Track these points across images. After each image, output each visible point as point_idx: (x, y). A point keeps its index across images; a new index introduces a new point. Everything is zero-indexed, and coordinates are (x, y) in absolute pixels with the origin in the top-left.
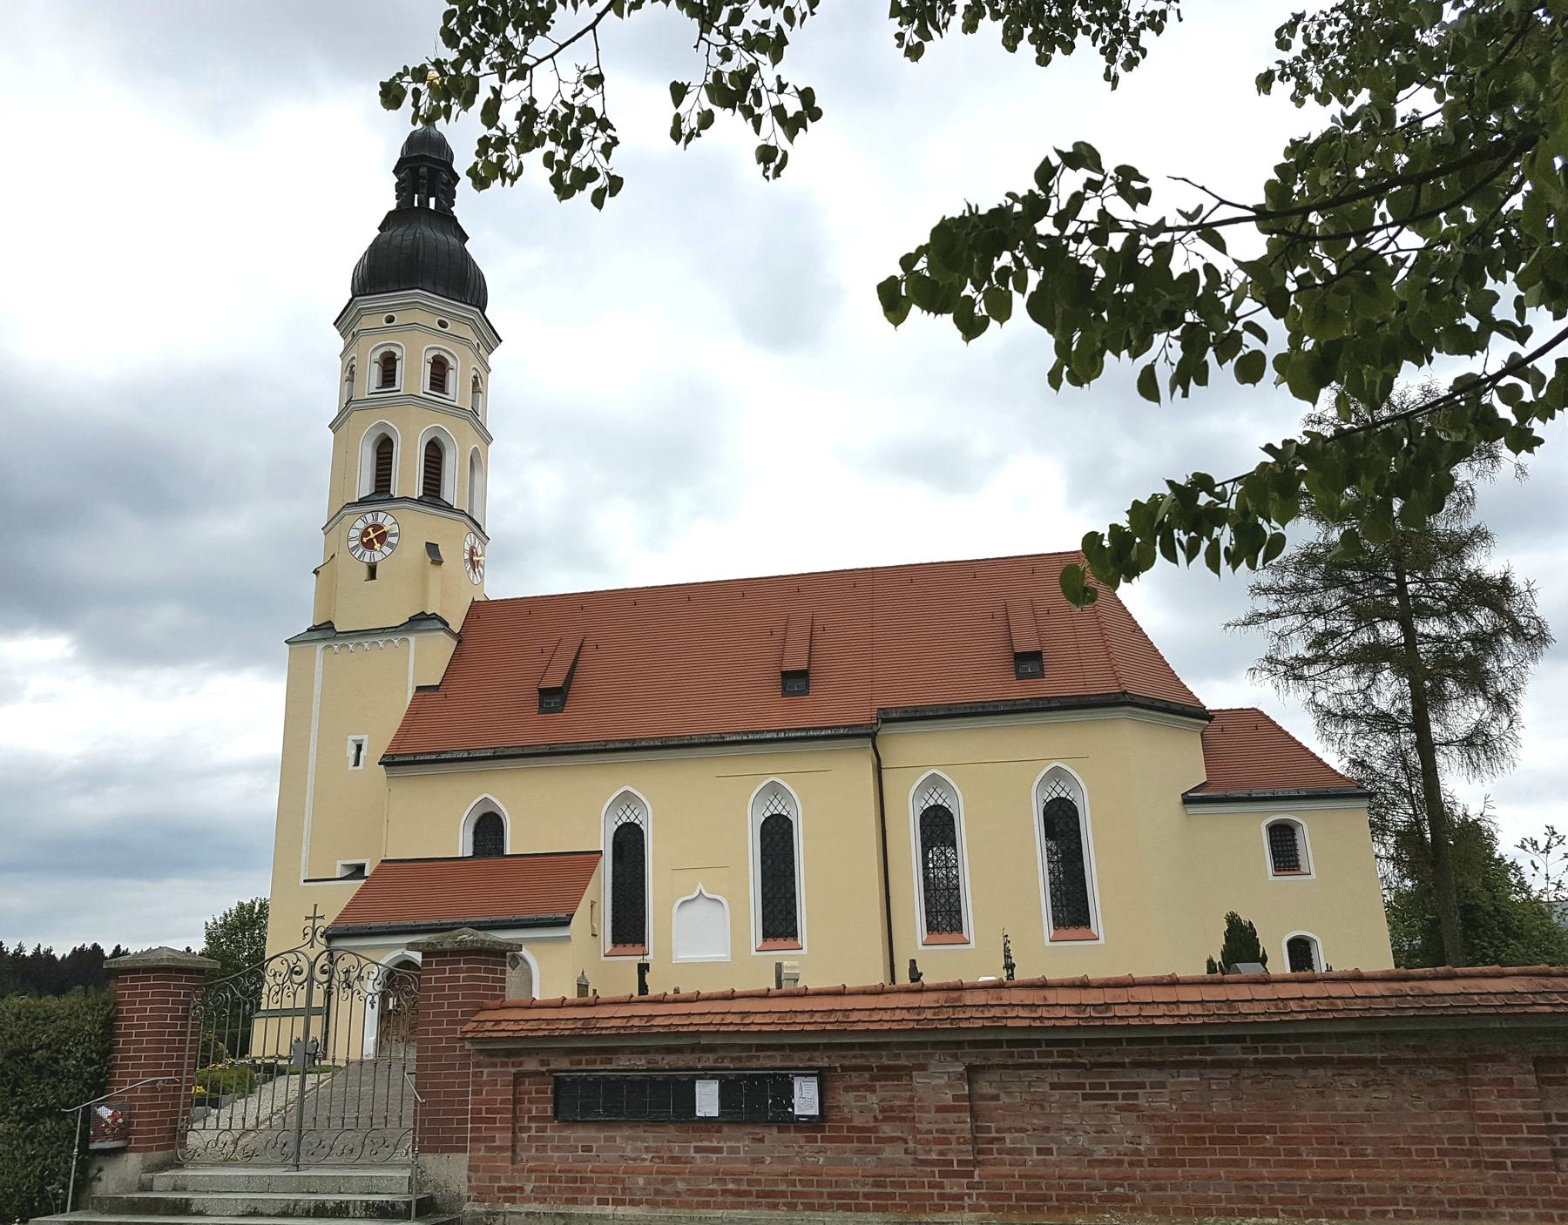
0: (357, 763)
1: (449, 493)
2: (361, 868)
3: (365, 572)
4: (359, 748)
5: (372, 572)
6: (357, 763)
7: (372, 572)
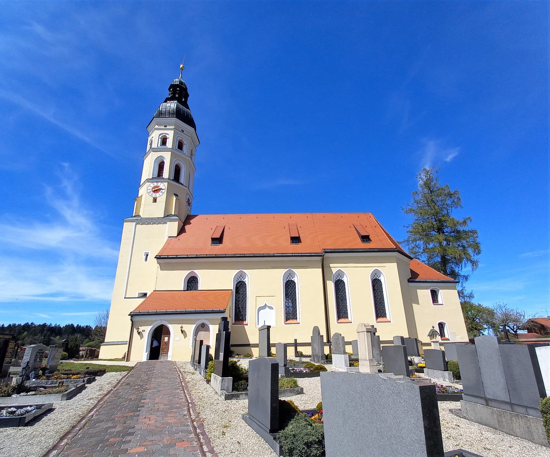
0: (146, 259)
1: (182, 179)
2: (145, 295)
4: (147, 255)
5: (155, 200)
6: (146, 259)
7: (155, 200)
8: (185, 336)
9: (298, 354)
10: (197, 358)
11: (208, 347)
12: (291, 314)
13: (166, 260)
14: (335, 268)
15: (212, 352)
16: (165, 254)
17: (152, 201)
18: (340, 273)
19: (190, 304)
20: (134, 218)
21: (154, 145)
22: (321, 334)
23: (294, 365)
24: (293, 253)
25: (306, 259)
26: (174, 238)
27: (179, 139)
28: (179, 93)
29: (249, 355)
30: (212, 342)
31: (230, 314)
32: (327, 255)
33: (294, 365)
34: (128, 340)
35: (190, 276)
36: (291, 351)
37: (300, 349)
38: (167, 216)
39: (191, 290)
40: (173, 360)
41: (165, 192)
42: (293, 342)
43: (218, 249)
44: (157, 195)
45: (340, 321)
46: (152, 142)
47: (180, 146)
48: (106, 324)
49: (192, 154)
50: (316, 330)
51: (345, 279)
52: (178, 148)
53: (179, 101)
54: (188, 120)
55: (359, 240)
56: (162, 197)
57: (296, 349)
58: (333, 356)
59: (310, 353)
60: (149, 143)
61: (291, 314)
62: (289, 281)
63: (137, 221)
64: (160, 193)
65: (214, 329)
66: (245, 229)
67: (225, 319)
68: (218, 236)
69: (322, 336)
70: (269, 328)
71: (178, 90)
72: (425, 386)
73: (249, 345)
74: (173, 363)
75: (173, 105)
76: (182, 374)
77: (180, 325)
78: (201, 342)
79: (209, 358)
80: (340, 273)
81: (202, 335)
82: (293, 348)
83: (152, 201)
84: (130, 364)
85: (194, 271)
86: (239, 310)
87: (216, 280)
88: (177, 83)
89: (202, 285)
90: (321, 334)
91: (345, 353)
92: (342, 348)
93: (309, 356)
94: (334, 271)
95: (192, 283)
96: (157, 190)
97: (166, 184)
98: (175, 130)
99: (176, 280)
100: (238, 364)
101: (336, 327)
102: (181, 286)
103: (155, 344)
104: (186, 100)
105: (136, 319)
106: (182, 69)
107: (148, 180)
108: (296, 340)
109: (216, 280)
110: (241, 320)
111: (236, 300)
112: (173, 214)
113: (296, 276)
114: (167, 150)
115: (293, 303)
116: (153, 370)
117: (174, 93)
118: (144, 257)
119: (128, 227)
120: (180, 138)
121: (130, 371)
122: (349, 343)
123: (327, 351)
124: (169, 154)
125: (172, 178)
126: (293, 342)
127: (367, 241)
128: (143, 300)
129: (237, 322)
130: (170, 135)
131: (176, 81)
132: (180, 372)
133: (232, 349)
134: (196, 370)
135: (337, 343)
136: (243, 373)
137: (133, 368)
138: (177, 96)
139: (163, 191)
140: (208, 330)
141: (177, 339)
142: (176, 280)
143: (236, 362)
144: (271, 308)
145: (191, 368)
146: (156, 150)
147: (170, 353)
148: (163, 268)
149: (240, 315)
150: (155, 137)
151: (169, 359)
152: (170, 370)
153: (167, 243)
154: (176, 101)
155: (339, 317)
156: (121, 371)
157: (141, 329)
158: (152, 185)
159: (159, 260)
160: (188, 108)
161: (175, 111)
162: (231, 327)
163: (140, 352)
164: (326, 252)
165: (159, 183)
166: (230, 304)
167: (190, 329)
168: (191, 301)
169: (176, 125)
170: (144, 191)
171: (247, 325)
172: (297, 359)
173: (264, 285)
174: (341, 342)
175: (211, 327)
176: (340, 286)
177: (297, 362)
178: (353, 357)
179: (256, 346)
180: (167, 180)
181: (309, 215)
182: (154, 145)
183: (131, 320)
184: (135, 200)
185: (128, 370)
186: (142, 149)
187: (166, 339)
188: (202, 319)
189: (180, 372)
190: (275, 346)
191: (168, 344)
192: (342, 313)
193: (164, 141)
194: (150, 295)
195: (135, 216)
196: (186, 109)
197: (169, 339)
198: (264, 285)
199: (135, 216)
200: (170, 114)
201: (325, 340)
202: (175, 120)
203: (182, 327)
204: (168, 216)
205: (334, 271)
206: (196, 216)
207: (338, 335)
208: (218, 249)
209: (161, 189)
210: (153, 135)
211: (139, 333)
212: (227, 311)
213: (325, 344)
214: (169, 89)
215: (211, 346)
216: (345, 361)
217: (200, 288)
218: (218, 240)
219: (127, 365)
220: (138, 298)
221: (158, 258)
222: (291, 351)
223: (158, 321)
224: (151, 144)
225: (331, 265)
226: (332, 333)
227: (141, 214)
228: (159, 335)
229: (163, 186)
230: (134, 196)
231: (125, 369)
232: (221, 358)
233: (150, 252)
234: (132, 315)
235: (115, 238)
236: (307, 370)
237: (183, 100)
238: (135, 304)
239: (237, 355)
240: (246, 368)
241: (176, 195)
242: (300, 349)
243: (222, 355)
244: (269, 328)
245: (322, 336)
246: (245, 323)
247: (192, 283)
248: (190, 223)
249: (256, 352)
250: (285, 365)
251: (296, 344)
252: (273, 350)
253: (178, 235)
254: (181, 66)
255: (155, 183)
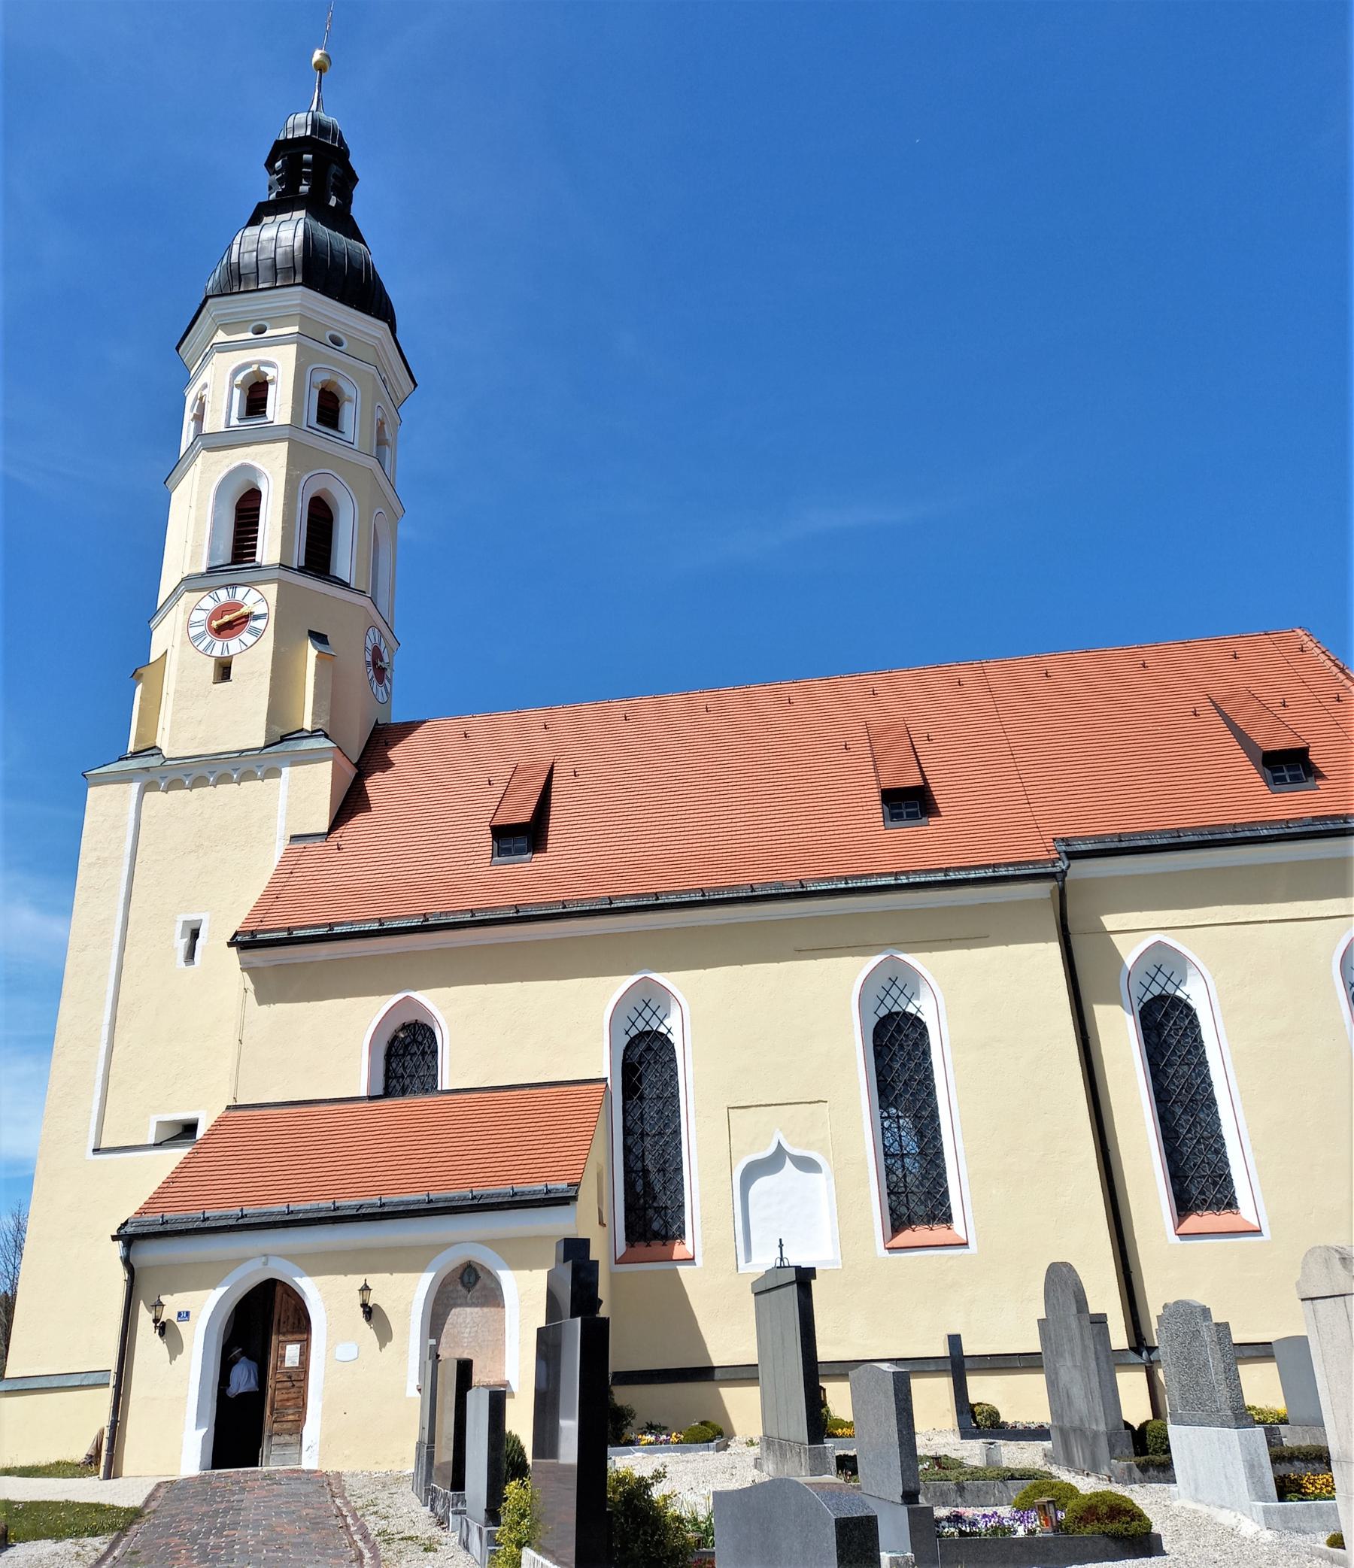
0: (190, 955)
1: (343, 564)
2: (189, 1129)
3: (210, 668)
4: (195, 934)
5: (224, 671)
6: (190, 955)
7: (224, 671)
8: (384, 1335)
9: (977, 1422)
10: (445, 1454)
11: (498, 1401)
12: (915, 1195)
13: (281, 951)
14: (1132, 934)
15: (520, 1422)
16: (277, 922)
17: (210, 677)
18: (1164, 961)
19: (398, 1167)
20: (133, 764)
21: (213, 423)
22: (1094, 1308)
23: (961, 1489)
24: (904, 871)
25: (966, 898)
26: (319, 843)
27: (321, 377)
28: (314, 172)
29: (712, 1433)
30: (516, 1367)
31: (597, 1219)
32: (1080, 870)
33: (961, 1489)
34: (113, 1366)
35: (397, 1024)
36: (932, 1399)
37: (982, 1389)
38: (283, 740)
39: (403, 1092)
40: (330, 1468)
41: (267, 627)
42: (942, 1350)
43: (526, 878)
44: (234, 645)
45: (1193, 1222)
46: (202, 407)
47: (330, 409)
48: (14, 1285)
49: (381, 442)
50: (1062, 1283)
51: (1194, 992)
52: (319, 420)
53: (316, 207)
54: (363, 291)
55: (1253, 778)
56: (254, 654)
57: (960, 1391)
58: (1178, 1436)
59: (1040, 1414)
60: (188, 415)
61: (915, 1195)
62: (891, 1016)
63: (148, 778)
64: (246, 637)
65: (525, 1295)
66: (639, 779)
67: (575, 1250)
68: (521, 813)
69: (1100, 1320)
70: (804, 1277)
71: (307, 164)
72: (341, 300)
73: (705, 1373)
74: (327, 1483)
75: (287, 232)
76: (374, 1549)
77: (358, 1280)
78: (465, 1369)
79: (506, 1463)
80: (1164, 961)
81: (463, 1318)
82: (944, 1385)
83: (210, 677)
84: (125, 1492)
85: (417, 995)
86: (648, 1185)
87: (527, 1034)
88: (300, 133)
89: (453, 1070)
90: (1094, 1308)
91: (1243, 1416)
92: (1223, 1393)
93: (1039, 1433)
94: (1130, 951)
95: (407, 1055)
96: (229, 624)
97: (271, 591)
98: (305, 341)
99: (332, 1044)
100: (657, 1492)
101: (1180, 1266)
102: (355, 1073)
103: (242, 1379)
104: (346, 199)
105: (149, 1254)
106: (321, 68)
107: (191, 583)
108: (955, 1341)
109: (527, 1034)
110: (656, 1236)
111: (627, 1132)
112: (308, 725)
113: (924, 990)
114: (272, 435)
115: (920, 1134)
116: (235, 1525)
117: (290, 178)
118: (182, 944)
119: (109, 807)
120: (327, 376)
121: (124, 1531)
122: (1261, 1351)
123: (1136, 1409)
124: (280, 452)
125: (298, 559)
126: (942, 1350)
127: (1296, 779)
128: (177, 1155)
129: (640, 1248)
130: (282, 364)
131: (299, 125)
132: (366, 1537)
133: (623, 1396)
134: (442, 1522)
135: (1191, 1366)
136: (686, 1545)
137: (135, 1514)
138: (304, 189)
139: (259, 624)
140: (493, 1297)
141: (346, 1351)
142: (332, 1044)
143: (643, 1485)
144: (807, 1165)
145: (411, 1513)
146: (218, 441)
147: (311, 1430)
148: (270, 988)
149: (652, 1213)
150: (215, 385)
151: (309, 1461)
152: (316, 1524)
153: (288, 868)
154: (301, 214)
155: (1184, 1205)
156: (78, 1535)
157: (173, 1304)
158: (209, 604)
159: (249, 954)
160: (355, 234)
161: (299, 255)
162: (613, 1276)
163: (171, 1435)
164: (1072, 856)
165: (241, 592)
166: (597, 1154)
167: (407, 1294)
168: (408, 1152)
169: (304, 320)
170: (176, 635)
171: (691, 1260)
172: (972, 1452)
173: (766, 1045)
174: (1214, 1360)
175: (510, 1280)
176: (1168, 1028)
177: (975, 1474)
178: (1292, 1438)
179: (744, 1375)
180: (276, 574)
181: (967, 672)
182: (213, 423)
183: (127, 1262)
184: (136, 676)
185: (113, 1527)
186: (157, 443)
187: (292, 1352)
188: (465, 1239)
189: (366, 1537)
190: (842, 1376)
191: (299, 1378)
192: (1199, 1179)
193: (255, 398)
194: (211, 1133)
195: (135, 755)
196: (341, 241)
197: (305, 1354)
198: (766, 1045)
199: (135, 755)
200: (280, 273)
201: (1119, 1338)
202: (299, 296)
203: (366, 1288)
204: (283, 739)
205: (1130, 951)
206: (408, 728)
207: (1189, 1316)
208: (526, 878)
209: (247, 617)
210: (206, 376)
211: (163, 1328)
212: (588, 1195)
213: (1117, 1361)
214: (269, 164)
215: (515, 1387)
216: (1252, 1467)
217: (447, 1080)
218: (523, 836)
219: (106, 1499)
220: (157, 1145)
221: (245, 942)
222: (932, 1399)
223: (256, 1260)
224: (199, 418)
225: (1111, 922)
226: (1155, 1301)
227: (162, 741)
228: (261, 1322)
229: (259, 599)
230: (135, 664)
231: (95, 1520)
232: (569, 1452)
233: (205, 917)
234: (129, 1238)
235: (55, 860)
236: (1035, 1522)
237: (333, 202)
238: (142, 1180)
239: (651, 1428)
240: (703, 1513)
241: (319, 638)
242: (982, 1389)
243: (569, 1427)
244: (804, 1277)
245: (1100, 1320)
246: (679, 1251)
247: (407, 1055)
248: (387, 765)
249: (742, 1406)
250: (910, 1497)
251: (957, 1365)
252: (839, 1399)
253: (339, 819)
254: (317, 56)
255: (223, 595)
